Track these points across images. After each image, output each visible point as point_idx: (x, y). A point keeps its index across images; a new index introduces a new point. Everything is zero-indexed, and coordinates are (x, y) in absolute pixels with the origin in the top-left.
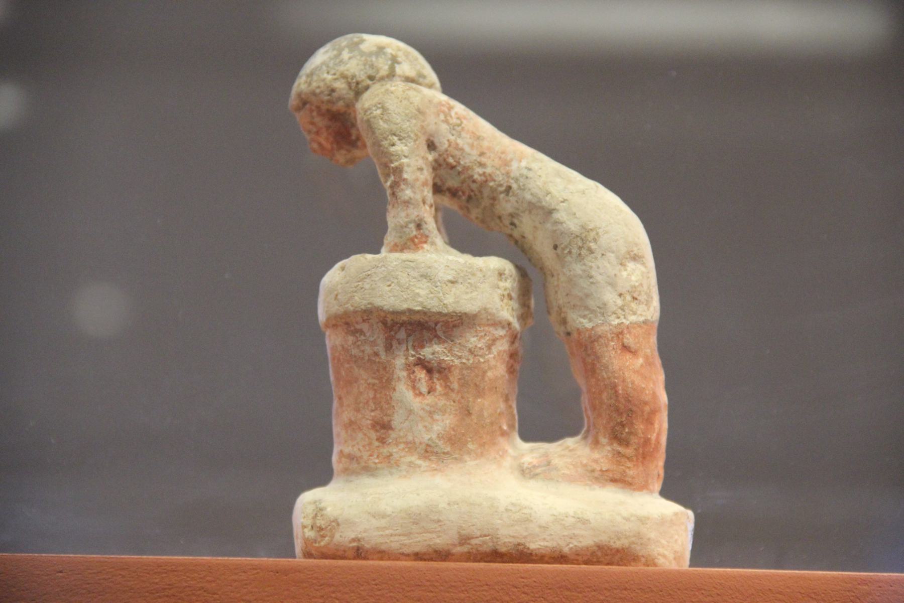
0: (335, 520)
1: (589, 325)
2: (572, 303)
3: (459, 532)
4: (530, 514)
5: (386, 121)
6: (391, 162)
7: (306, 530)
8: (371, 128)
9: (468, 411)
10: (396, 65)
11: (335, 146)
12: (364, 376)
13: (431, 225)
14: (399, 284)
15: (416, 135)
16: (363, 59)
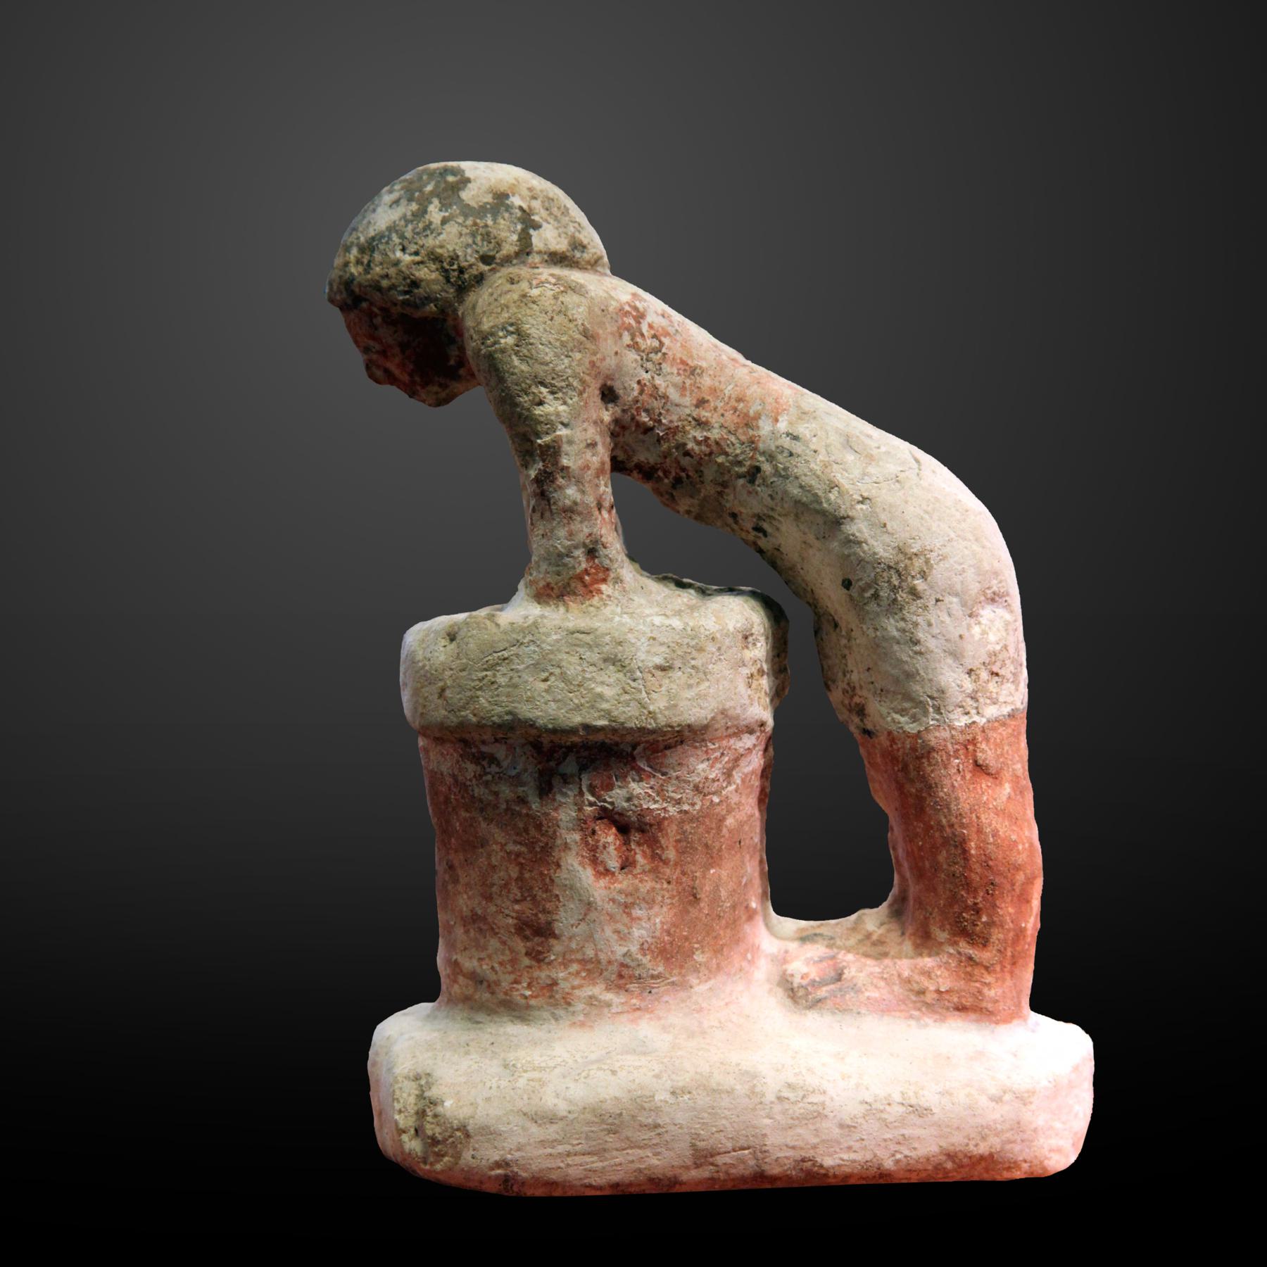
0: (463, 1128)
1: (912, 728)
2: (878, 686)
3: (693, 1145)
4: (823, 1104)
5: (523, 359)
6: (538, 436)
7: (405, 1137)
8: (497, 370)
9: (695, 896)
10: (531, 232)
11: (417, 379)
12: (499, 840)
13: (614, 547)
14: (563, 677)
15: (582, 381)
16: (469, 222)
